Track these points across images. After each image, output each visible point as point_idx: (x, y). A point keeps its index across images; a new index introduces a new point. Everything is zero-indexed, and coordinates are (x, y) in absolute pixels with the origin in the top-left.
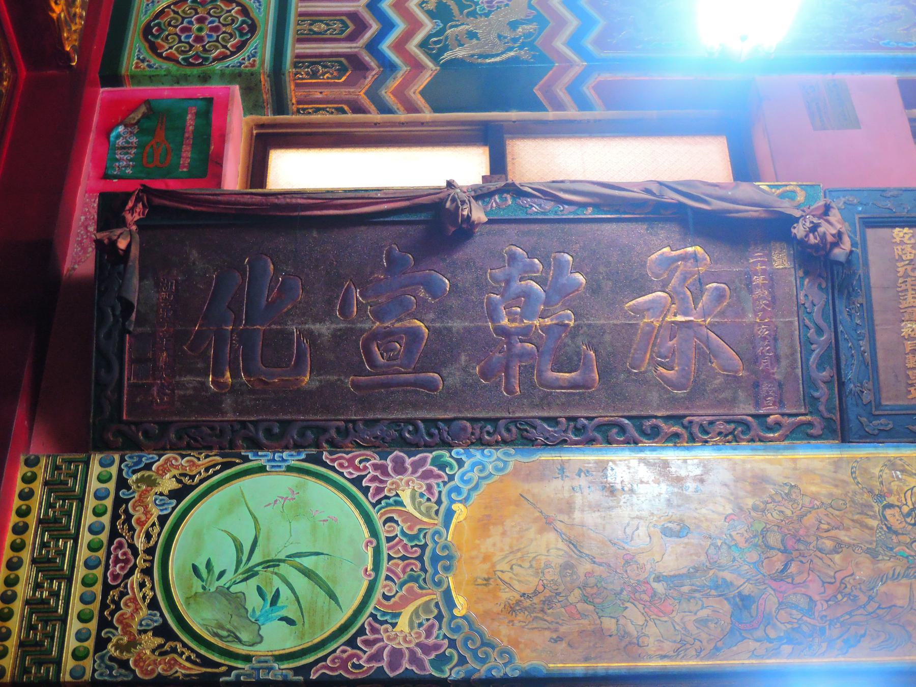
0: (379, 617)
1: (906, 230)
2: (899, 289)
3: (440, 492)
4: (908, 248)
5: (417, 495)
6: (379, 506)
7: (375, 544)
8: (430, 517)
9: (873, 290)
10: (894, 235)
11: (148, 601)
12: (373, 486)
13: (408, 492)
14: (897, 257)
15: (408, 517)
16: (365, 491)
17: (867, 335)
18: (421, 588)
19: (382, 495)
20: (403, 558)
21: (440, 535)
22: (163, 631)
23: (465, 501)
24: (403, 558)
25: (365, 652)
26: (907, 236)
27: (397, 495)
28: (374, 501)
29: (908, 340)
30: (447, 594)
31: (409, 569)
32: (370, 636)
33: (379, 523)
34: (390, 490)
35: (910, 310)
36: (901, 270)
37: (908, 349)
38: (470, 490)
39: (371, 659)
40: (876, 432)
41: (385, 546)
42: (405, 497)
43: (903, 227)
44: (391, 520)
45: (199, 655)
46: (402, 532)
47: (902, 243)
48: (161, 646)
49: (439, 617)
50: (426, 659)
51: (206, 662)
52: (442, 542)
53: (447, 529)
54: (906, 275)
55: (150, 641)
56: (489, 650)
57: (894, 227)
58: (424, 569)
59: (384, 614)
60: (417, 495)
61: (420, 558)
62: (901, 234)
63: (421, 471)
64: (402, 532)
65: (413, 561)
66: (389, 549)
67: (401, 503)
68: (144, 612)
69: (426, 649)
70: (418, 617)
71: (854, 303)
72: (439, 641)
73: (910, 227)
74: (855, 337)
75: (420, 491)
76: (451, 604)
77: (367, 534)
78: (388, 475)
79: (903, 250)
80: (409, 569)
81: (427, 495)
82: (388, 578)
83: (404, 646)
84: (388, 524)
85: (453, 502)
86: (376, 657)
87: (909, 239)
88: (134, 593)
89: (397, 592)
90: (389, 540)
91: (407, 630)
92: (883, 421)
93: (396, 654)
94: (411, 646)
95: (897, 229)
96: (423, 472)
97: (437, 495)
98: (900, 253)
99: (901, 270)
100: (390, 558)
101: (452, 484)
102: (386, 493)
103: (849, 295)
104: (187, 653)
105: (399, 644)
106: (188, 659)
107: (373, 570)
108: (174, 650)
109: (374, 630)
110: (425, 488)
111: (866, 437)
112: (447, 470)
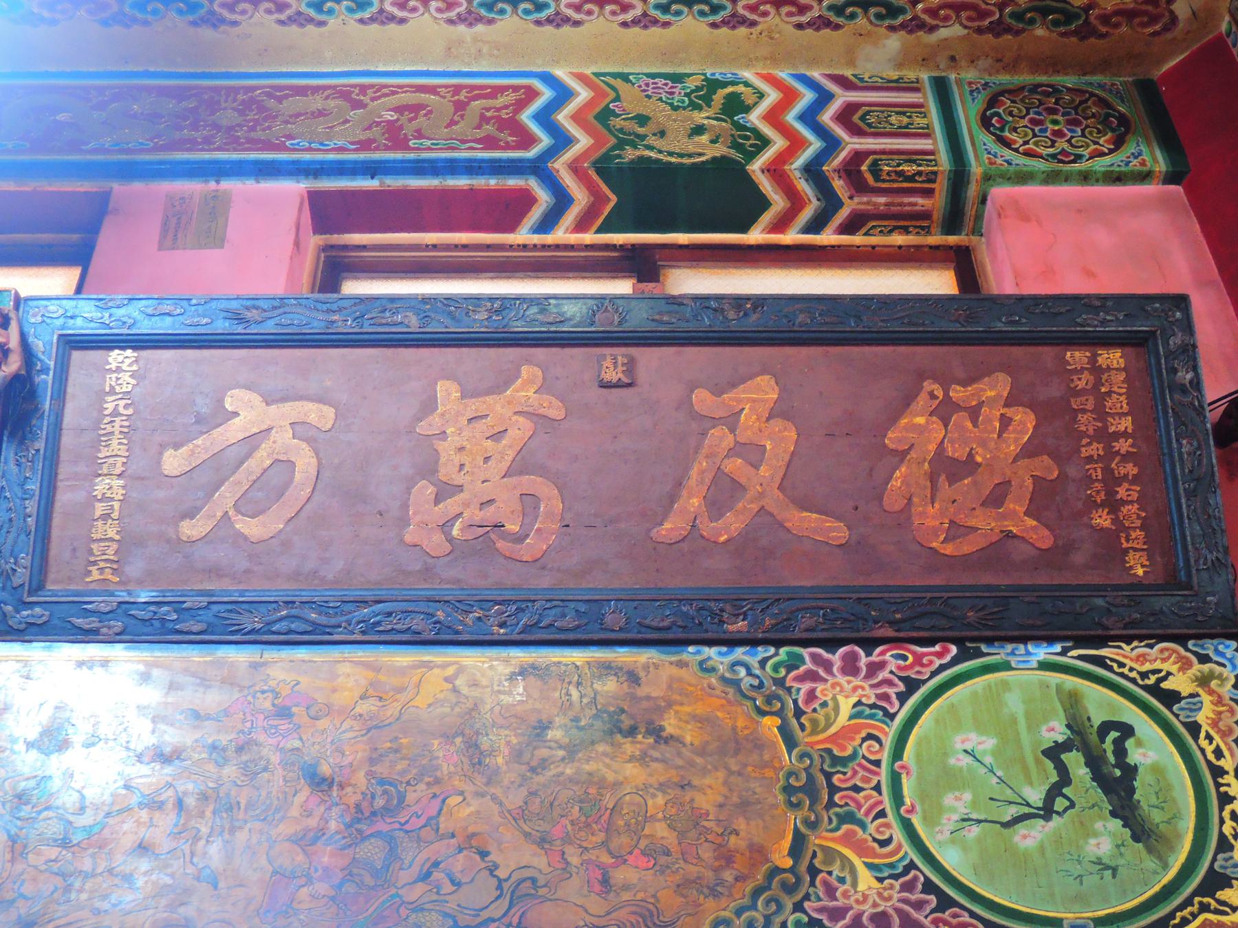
0: (881, 713)
1: (129, 352)
2: (103, 432)
3: (812, 884)
4: (126, 377)
5: (848, 879)
6: (905, 863)
7: (902, 810)
8: (825, 849)
9: (64, 432)
10: (110, 359)
11: (1203, 735)
12: (916, 896)
13: (862, 887)
14: (107, 389)
15: (861, 849)
16: (929, 887)
17: (37, 493)
18: (829, 751)
19: (902, 880)
20: (857, 789)
21: (806, 822)
22: (1171, 698)
23: (776, 871)
24: (857, 789)
25: (891, 672)
26: (128, 361)
27: (880, 880)
28: (913, 872)
29: (100, 501)
30: (791, 743)
31: (849, 774)
32: (892, 691)
33: (898, 835)
34: (892, 887)
35: (112, 460)
36: (110, 407)
37: (98, 513)
38: (768, 888)
39: (882, 665)
40: (23, 626)
41: (887, 804)
42: (866, 880)
43: (123, 348)
44: (884, 843)
45: (1110, 669)
46: (863, 826)
47: (119, 370)
48: (1165, 678)
49: (799, 713)
50: (809, 665)
51: (1100, 661)
52: (805, 811)
53: (796, 831)
54: (115, 413)
55: (1180, 683)
56: (727, 675)
57: (112, 348)
58: (828, 776)
59: (872, 717)
60: (848, 879)
61: (833, 789)
62: (120, 359)
63: (847, 920)
64: (863, 826)
65: (844, 786)
66: (881, 802)
67: (870, 866)
68: (1201, 718)
69: (812, 676)
70: (827, 717)
71: (27, 450)
72: (796, 685)
73: (134, 348)
74: (20, 494)
75: (845, 887)
76: (784, 730)
77: (916, 821)
78: (897, 910)
79: (118, 379)
80: (849, 774)
81: (833, 880)
82: (877, 763)
83: (842, 680)
84: (886, 836)
85: (792, 870)
86: (874, 668)
87: (130, 365)
88: (1226, 744)
89: (860, 746)
90: (882, 814)
91: (840, 698)
92: (38, 610)
93: (850, 668)
94: (831, 680)
95: (117, 351)
96: (844, 918)
97: (818, 882)
98: (113, 384)
99: (110, 407)
100: (877, 788)
101: (798, 897)
102: (897, 885)
103: (22, 441)
104: (1126, 671)
105: (849, 682)
106: (1122, 665)
107: (900, 774)
108: (1144, 675)
109: (885, 697)
110: (838, 894)
111: (7, 633)
112: (806, 919)
